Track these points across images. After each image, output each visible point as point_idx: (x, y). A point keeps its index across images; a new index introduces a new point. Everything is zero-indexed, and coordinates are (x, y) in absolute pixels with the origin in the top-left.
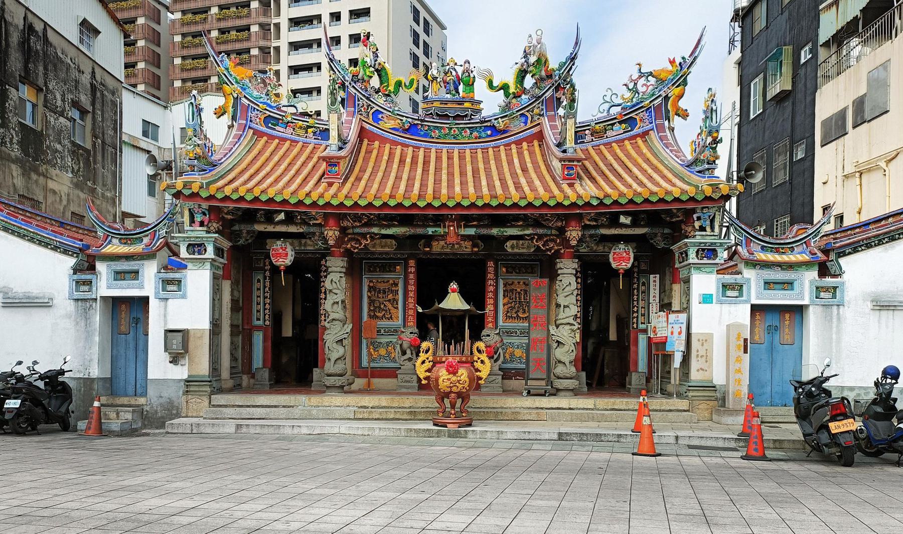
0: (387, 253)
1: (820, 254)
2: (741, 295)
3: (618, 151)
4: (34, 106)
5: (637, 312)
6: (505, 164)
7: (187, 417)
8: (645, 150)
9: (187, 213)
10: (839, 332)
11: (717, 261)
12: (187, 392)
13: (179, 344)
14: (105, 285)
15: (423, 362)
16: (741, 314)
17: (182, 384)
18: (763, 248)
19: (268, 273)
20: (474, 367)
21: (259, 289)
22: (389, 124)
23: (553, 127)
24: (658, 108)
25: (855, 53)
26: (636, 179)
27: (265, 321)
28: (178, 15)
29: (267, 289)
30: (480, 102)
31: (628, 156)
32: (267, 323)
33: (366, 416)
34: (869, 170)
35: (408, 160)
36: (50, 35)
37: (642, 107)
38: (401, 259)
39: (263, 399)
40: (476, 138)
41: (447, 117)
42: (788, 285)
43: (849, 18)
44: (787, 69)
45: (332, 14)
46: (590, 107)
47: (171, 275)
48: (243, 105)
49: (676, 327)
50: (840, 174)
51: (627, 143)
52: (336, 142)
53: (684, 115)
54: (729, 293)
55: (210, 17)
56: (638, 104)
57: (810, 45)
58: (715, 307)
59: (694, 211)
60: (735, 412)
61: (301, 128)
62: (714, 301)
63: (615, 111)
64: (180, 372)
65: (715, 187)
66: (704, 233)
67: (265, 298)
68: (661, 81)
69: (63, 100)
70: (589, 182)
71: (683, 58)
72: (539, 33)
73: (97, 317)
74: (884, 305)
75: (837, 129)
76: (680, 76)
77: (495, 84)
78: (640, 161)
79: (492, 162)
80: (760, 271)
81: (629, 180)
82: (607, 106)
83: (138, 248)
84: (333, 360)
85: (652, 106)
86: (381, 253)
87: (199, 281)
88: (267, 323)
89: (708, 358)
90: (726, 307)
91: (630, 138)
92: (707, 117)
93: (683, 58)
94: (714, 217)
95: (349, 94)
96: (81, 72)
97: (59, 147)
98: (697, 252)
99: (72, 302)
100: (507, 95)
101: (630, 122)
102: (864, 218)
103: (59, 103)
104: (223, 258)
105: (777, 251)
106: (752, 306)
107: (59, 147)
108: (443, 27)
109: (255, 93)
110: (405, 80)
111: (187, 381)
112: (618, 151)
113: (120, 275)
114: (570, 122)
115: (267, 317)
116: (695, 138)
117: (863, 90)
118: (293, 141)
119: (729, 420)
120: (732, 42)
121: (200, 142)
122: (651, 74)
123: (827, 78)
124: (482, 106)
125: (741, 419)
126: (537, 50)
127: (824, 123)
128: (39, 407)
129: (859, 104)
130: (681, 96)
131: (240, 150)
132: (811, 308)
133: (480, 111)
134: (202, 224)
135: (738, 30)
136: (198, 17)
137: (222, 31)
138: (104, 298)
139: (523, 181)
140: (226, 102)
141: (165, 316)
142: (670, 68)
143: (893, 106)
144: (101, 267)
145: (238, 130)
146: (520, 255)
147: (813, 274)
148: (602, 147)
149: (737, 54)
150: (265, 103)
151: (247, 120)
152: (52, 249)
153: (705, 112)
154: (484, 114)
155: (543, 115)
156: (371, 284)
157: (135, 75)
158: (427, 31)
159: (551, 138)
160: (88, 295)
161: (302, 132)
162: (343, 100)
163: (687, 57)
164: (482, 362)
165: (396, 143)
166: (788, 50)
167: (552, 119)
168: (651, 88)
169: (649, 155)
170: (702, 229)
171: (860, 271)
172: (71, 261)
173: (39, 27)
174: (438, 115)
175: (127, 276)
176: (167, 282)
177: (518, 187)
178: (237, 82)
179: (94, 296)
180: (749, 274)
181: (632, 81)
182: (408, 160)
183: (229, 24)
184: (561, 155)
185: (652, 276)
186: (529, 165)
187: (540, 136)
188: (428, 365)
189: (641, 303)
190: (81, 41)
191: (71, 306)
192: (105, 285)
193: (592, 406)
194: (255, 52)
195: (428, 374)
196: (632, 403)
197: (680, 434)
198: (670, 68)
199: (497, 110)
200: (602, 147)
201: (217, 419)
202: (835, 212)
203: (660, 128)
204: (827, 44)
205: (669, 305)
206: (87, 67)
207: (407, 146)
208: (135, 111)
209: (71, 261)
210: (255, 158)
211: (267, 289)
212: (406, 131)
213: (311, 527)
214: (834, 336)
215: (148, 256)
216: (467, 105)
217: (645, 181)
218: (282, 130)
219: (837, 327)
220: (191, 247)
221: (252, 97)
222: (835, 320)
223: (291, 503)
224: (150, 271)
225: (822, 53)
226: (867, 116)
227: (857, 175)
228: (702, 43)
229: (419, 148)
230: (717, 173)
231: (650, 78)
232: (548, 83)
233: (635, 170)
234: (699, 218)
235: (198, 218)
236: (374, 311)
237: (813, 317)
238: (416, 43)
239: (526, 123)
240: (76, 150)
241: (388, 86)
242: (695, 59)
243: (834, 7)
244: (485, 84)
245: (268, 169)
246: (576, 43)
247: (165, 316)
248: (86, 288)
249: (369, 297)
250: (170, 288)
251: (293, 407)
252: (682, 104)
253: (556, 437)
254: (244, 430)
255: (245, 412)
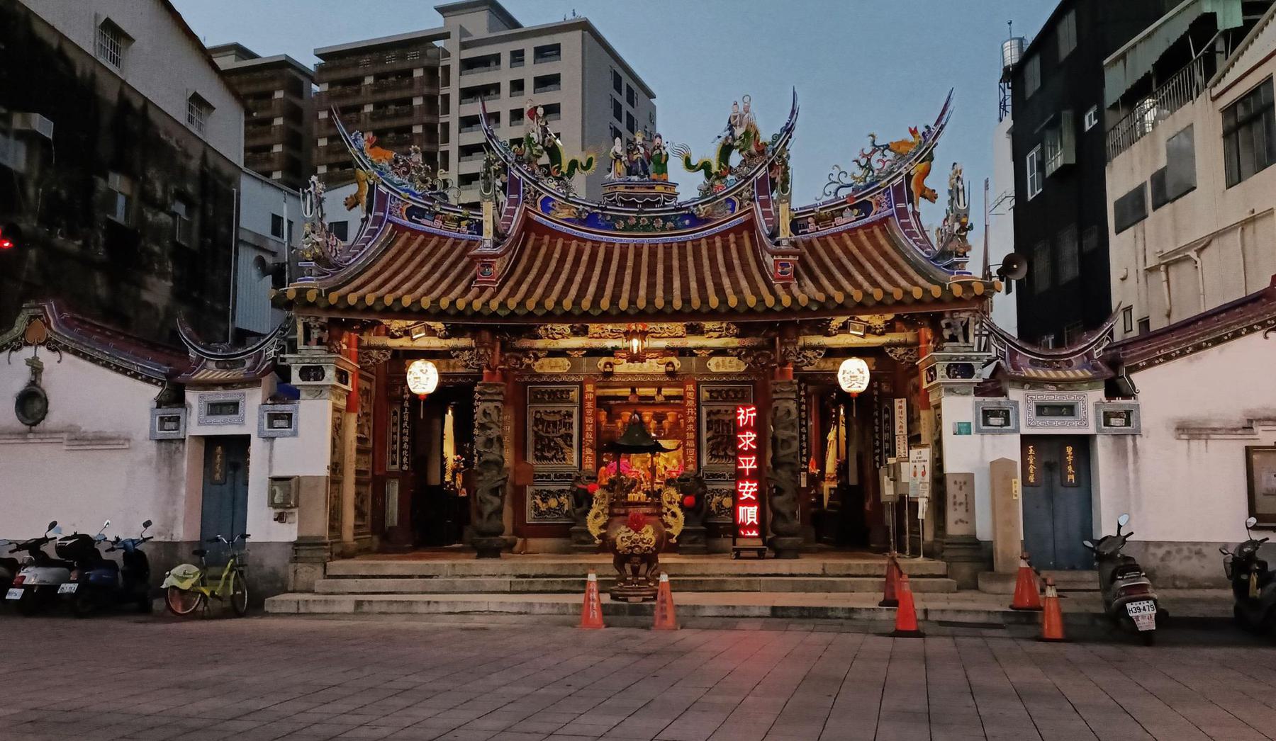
0: (558, 375)
1: (1105, 369)
2: (1007, 423)
3: (849, 243)
4: (128, 199)
5: (881, 447)
6: (706, 262)
7: (294, 592)
8: (883, 241)
9: (300, 328)
10: (1137, 471)
11: (974, 379)
12: (295, 560)
13: (287, 494)
14: (197, 421)
15: (597, 516)
16: (1009, 447)
17: (290, 547)
18: (1032, 361)
19: (406, 404)
20: (662, 521)
21: (395, 424)
22: (564, 214)
23: (765, 214)
24: (898, 189)
25: (1150, 117)
26: (868, 277)
27: (402, 464)
28: (325, 87)
29: (405, 424)
30: (675, 185)
31: (861, 248)
32: (405, 467)
33: (526, 587)
34: (1177, 262)
35: (585, 258)
36: (152, 113)
37: (879, 188)
38: (574, 383)
39: (393, 565)
40: (671, 229)
41: (634, 204)
42: (1069, 410)
43: (1140, 75)
44: (1069, 138)
45: (512, 83)
46: (807, 190)
47: (280, 408)
48: (380, 193)
49: (919, 465)
50: (1141, 268)
51: (860, 232)
52: (491, 236)
53: (932, 196)
54: (993, 421)
55: (363, 89)
56: (872, 184)
57: (1095, 108)
58: (975, 438)
59: (941, 315)
60: (1005, 577)
61: (452, 220)
62: (973, 430)
63: (843, 193)
64: (289, 533)
65: (967, 286)
66: (955, 344)
67: (402, 435)
68: (901, 157)
69: (165, 191)
70: (808, 282)
71: (927, 127)
72: (747, 99)
73: (189, 463)
74: (1189, 430)
75: (1133, 210)
76: (923, 148)
77: (693, 163)
78: (875, 254)
79: (690, 259)
80: (1031, 392)
81: (860, 278)
82: (833, 187)
83: (238, 373)
84: (486, 515)
85: (895, 183)
86: (551, 375)
87: (315, 414)
88: (405, 467)
89: (969, 506)
90: (988, 438)
91: (864, 227)
92: (953, 199)
93: (927, 127)
94: (968, 323)
95: (512, 176)
96: (188, 157)
97: (157, 249)
98: (948, 369)
99: (154, 444)
100: (708, 175)
101: (865, 207)
102: (1175, 319)
103: (159, 194)
104: (346, 384)
105: (1050, 366)
106: (1022, 436)
107: (157, 249)
108: (651, 95)
109: (396, 179)
110: (582, 159)
111: (295, 544)
112: (849, 243)
113: (216, 409)
114: (783, 208)
115: (405, 460)
116: (940, 225)
117: (1162, 163)
118: (441, 237)
119: (998, 587)
120: (1003, 106)
121: (319, 240)
122: (887, 147)
123: (1119, 149)
124: (677, 190)
125: (1013, 586)
126: (745, 120)
127: (1118, 204)
128: (105, 583)
129: (1159, 179)
130: (926, 173)
131: (373, 247)
132: (1099, 440)
133: (674, 196)
134: (320, 342)
135: (1009, 92)
136: (348, 90)
137: (378, 106)
138: (197, 438)
139: (726, 282)
140: (360, 190)
141: (270, 461)
142: (911, 139)
143: (1200, 183)
144: (191, 397)
145: (373, 224)
146: (727, 374)
147: (1099, 394)
148: (830, 239)
149: (1008, 122)
150: (407, 191)
151: (385, 212)
152: (131, 376)
153: (950, 192)
154: (681, 199)
155: (753, 200)
156: (538, 416)
157: (269, 160)
158: (631, 99)
159: (763, 227)
160: (173, 435)
161: (453, 226)
162: (504, 185)
163: (932, 125)
164: (674, 515)
165: (569, 237)
166: (1067, 115)
167: (765, 204)
168: (888, 164)
169: (888, 248)
170: (953, 338)
171: (1162, 389)
172: (155, 391)
173: (137, 104)
174: (622, 201)
175: (224, 408)
176: (273, 417)
177: (720, 290)
178: (374, 166)
179: (181, 436)
180: (1015, 394)
181: (864, 156)
182: (585, 258)
183: (388, 96)
184: (774, 248)
185: (896, 401)
186: (736, 262)
187: (750, 225)
188: (602, 520)
189: (885, 436)
190: (190, 119)
191: (152, 448)
192: (197, 421)
193: (819, 572)
194: (418, 130)
195: (603, 531)
196: (878, 564)
197: (930, 606)
198: (911, 139)
199: (696, 194)
200: (830, 239)
201: (332, 593)
202: (1136, 315)
203: (902, 213)
204: (1115, 107)
205: (918, 438)
206: (196, 151)
207: (585, 240)
208: (257, 203)
209: (155, 391)
210: (394, 259)
211: (405, 424)
212: (582, 222)
213: (402, 734)
214: (1131, 476)
215: (253, 382)
216: (659, 189)
217: (880, 279)
218: (428, 223)
219: (1135, 462)
220: (305, 373)
221: (392, 183)
222: (1130, 455)
223: (391, 701)
224: (254, 401)
225: (1111, 118)
226: (1170, 194)
227: (1162, 268)
228: (950, 108)
229: (600, 243)
230: (968, 268)
231: (887, 152)
232: (758, 161)
233: (869, 266)
234: (948, 326)
235: (315, 334)
236: (542, 450)
237: (1103, 451)
238: (618, 115)
239: (733, 209)
240: (178, 253)
241: (560, 168)
242: (942, 128)
243: (1121, 63)
244: (681, 162)
245: (407, 272)
246: (793, 111)
247: (270, 461)
248: (172, 425)
249: (536, 433)
250: (277, 423)
251: (431, 577)
252: (929, 183)
253: (768, 612)
254: (366, 608)
255: (369, 584)
